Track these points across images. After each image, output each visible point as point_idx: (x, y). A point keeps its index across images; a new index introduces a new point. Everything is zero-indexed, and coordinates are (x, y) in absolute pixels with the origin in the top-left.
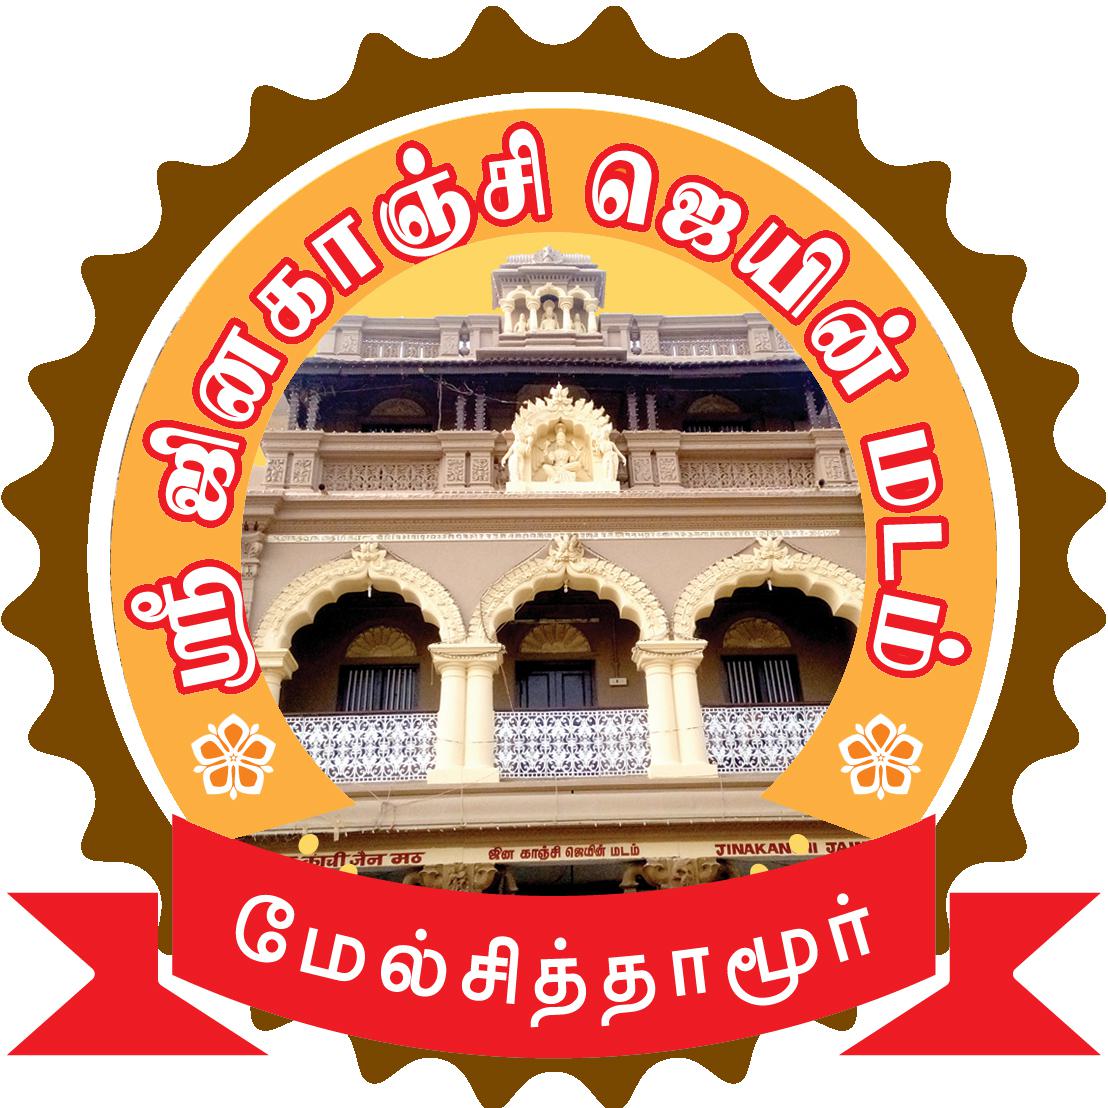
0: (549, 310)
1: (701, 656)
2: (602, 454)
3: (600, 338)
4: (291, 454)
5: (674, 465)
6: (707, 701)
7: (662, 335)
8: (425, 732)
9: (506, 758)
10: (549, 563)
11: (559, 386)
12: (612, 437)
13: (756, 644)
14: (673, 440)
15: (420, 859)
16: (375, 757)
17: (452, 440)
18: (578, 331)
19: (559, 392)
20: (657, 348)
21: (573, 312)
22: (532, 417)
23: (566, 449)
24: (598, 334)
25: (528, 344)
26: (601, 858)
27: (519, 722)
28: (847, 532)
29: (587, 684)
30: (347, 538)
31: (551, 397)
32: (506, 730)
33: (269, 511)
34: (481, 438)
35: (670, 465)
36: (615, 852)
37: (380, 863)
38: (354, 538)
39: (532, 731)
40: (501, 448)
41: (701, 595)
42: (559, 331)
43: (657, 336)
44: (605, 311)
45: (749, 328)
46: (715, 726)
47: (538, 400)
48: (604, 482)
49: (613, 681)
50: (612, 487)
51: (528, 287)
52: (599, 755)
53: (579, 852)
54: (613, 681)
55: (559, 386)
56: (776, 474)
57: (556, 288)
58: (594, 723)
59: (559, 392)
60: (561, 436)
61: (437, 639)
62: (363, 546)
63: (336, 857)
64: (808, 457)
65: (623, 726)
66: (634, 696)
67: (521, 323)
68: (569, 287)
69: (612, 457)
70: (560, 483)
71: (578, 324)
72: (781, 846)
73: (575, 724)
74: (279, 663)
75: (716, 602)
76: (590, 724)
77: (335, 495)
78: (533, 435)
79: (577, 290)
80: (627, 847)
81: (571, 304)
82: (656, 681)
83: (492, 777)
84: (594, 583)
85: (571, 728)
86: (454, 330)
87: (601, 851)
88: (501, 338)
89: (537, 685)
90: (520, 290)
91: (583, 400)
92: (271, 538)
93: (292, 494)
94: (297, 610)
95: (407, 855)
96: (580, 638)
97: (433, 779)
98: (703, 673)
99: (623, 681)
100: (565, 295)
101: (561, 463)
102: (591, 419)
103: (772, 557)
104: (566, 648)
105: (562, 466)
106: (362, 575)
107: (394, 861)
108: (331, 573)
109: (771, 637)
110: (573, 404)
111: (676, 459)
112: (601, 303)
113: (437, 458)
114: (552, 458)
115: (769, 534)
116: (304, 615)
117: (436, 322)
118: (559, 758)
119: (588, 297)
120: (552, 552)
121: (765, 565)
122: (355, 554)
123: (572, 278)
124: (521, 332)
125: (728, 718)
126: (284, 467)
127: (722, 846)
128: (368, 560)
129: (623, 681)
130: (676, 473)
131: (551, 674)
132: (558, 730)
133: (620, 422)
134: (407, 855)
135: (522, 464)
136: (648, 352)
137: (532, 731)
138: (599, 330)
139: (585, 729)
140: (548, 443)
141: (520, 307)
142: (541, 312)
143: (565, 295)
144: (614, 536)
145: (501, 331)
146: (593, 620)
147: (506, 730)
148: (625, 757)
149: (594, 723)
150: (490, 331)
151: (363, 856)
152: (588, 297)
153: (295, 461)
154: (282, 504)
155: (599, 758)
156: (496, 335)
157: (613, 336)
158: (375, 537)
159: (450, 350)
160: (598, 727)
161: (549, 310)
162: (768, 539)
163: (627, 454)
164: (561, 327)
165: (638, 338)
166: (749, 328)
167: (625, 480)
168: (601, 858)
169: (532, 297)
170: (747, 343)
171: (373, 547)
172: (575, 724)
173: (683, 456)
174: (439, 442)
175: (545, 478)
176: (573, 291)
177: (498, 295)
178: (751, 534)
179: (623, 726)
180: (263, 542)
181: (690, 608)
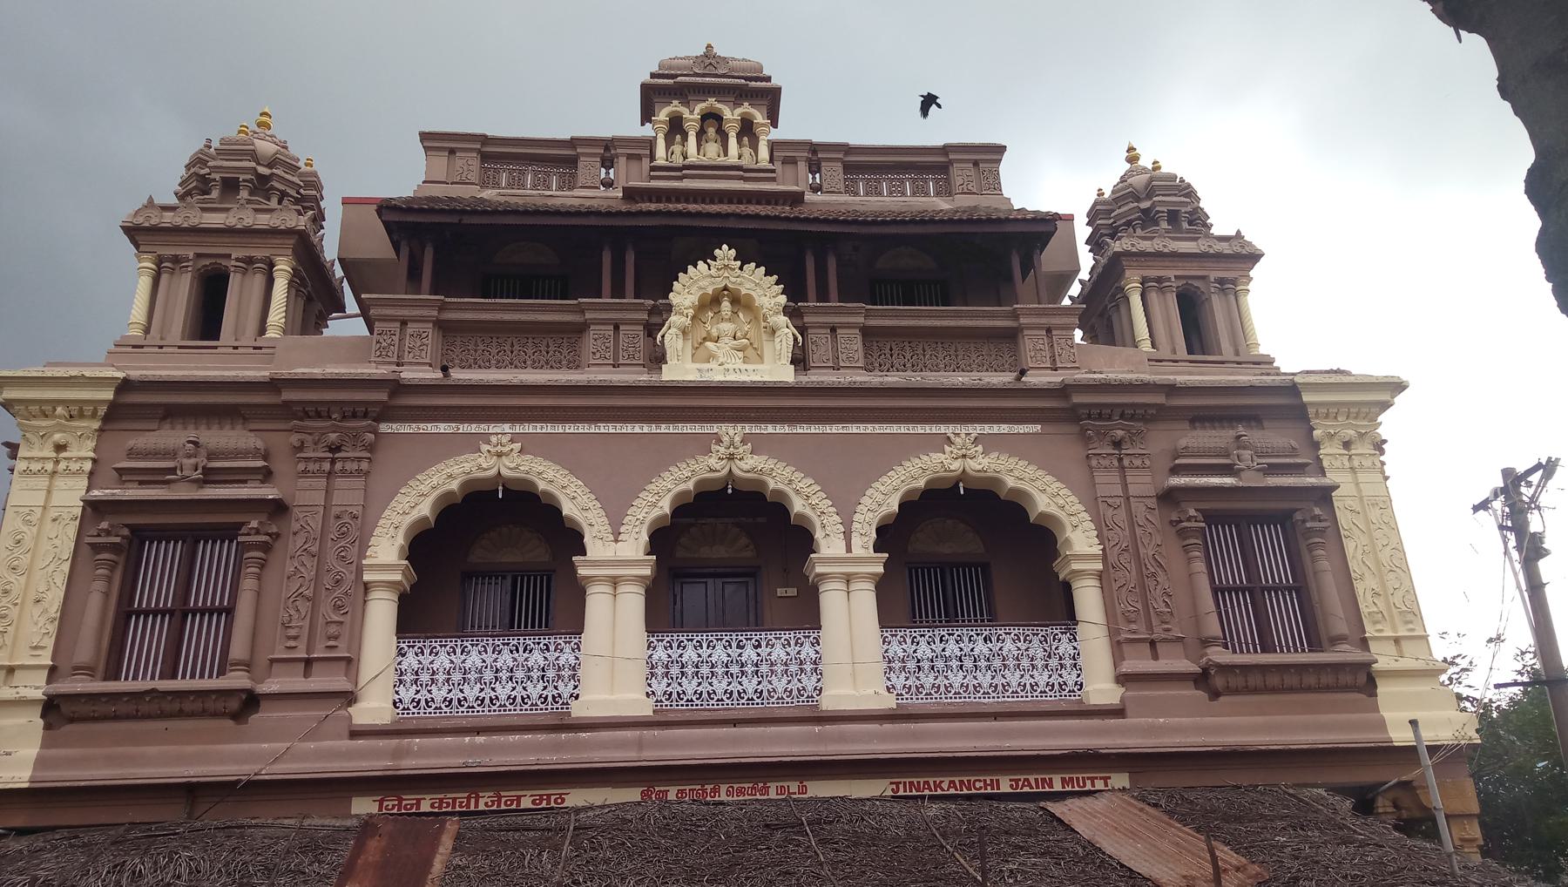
0: (711, 131)
1: (881, 569)
2: (774, 332)
3: (773, 171)
4: (404, 323)
5: (858, 344)
6: (887, 619)
7: (849, 168)
8: (567, 657)
9: (660, 687)
10: (712, 461)
11: (725, 247)
12: (786, 311)
13: (946, 549)
14: (858, 315)
15: (563, 801)
16: (435, 666)
17: (596, 308)
18: (746, 162)
19: (725, 253)
20: (841, 186)
21: (739, 137)
22: (688, 289)
23: (729, 330)
24: (771, 167)
25: (685, 177)
26: (655, 378)
27: (675, 645)
28: (1050, 428)
29: (751, 592)
30: (473, 428)
31: (714, 259)
32: (660, 654)
33: (382, 396)
34: (635, 308)
35: (852, 344)
36: (780, 790)
37: (519, 804)
38: (483, 428)
39: (690, 654)
40: (655, 320)
41: (883, 498)
42: (722, 160)
43: (841, 170)
44: (776, 134)
45: (951, 162)
46: (896, 649)
47: (700, 263)
48: (776, 369)
49: (780, 592)
50: (784, 373)
51: (686, 103)
52: (765, 683)
53: (741, 792)
54: (780, 592)
55: (725, 247)
56: (974, 356)
57: (719, 106)
58: (759, 646)
59: (725, 253)
60: (726, 305)
61: (582, 551)
62: (494, 439)
63: (469, 798)
64: (1011, 337)
65: (793, 650)
66: (806, 615)
67: (677, 148)
68: (737, 104)
69: (787, 333)
70: (727, 368)
71: (747, 151)
72: (961, 782)
73: (739, 647)
74: (398, 577)
75: (900, 506)
76: (756, 647)
77: (459, 375)
78: (693, 307)
79: (746, 108)
80: (794, 786)
81: (737, 126)
82: (832, 601)
83: (645, 709)
84: (763, 484)
85: (734, 652)
86: (594, 155)
87: (766, 790)
88: (653, 169)
89: (694, 595)
90: (676, 106)
91: (753, 265)
92: (384, 428)
93: (409, 374)
94: (415, 515)
95: (549, 796)
96: (744, 541)
97: (578, 710)
98: (883, 587)
99: (792, 592)
100: (731, 114)
101: (726, 340)
102: (765, 291)
103: (964, 456)
104: (732, 558)
105: (727, 343)
106: (493, 472)
107: (533, 802)
108: (456, 470)
109: (963, 543)
110: (741, 268)
111: (859, 338)
112: (775, 124)
113: (581, 329)
114: (714, 333)
115: (962, 429)
116: (425, 519)
117: (573, 142)
118: (720, 686)
119: (759, 117)
120: (714, 447)
121: (956, 465)
122: (485, 447)
123: (738, 94)
124: (678, 160)
125: (909, 641)
126: (396, 338)
127: (897, 784)
128: (500, 455)
129: (792, 592)
130: (861, 353)
131: (710, 581)
132: (719, 654)
133: (794, 290)
134: (549, 796)
135: (680, 341)
136: (831, 197)
137: (690, 654)
138: (771, 161)
139: (749, 653)
140: (711, 314)
141: (676, 127)
142: (701, 134)
143: (731, 114)
144: (787, 429)
145: (652, 157)
146: (760, 520)
147: (660, 654)
148: (794, 685)
149: (759, 646)
150: (639, 157)
151: (500, 797)
152: (759, 117)
153: (409, 331)
154: (397, 387)
155: (765, 686)
156: (646, 163)
157: (789, 168)
158: (506, 427)
159: (594, 192)
160: (764, 651)
161: (711, 131)
162: (963, 433)
163: (802, 330)
164: (726, 154)
165: (819, 171)
166: (951, 162)
167: (800, 360)
168: (655, 378)
169: (692, 116)
170: (947, 181)
171: (505, 440)
172: (739, 647)
173: (867, 333)
174: (583, 312)
175: (710, 357)
176: (739, 111)
177: (647, 115)
178: (942, 428)
179: (793, 650)
180: (375, 432)
181: (870, 515)
